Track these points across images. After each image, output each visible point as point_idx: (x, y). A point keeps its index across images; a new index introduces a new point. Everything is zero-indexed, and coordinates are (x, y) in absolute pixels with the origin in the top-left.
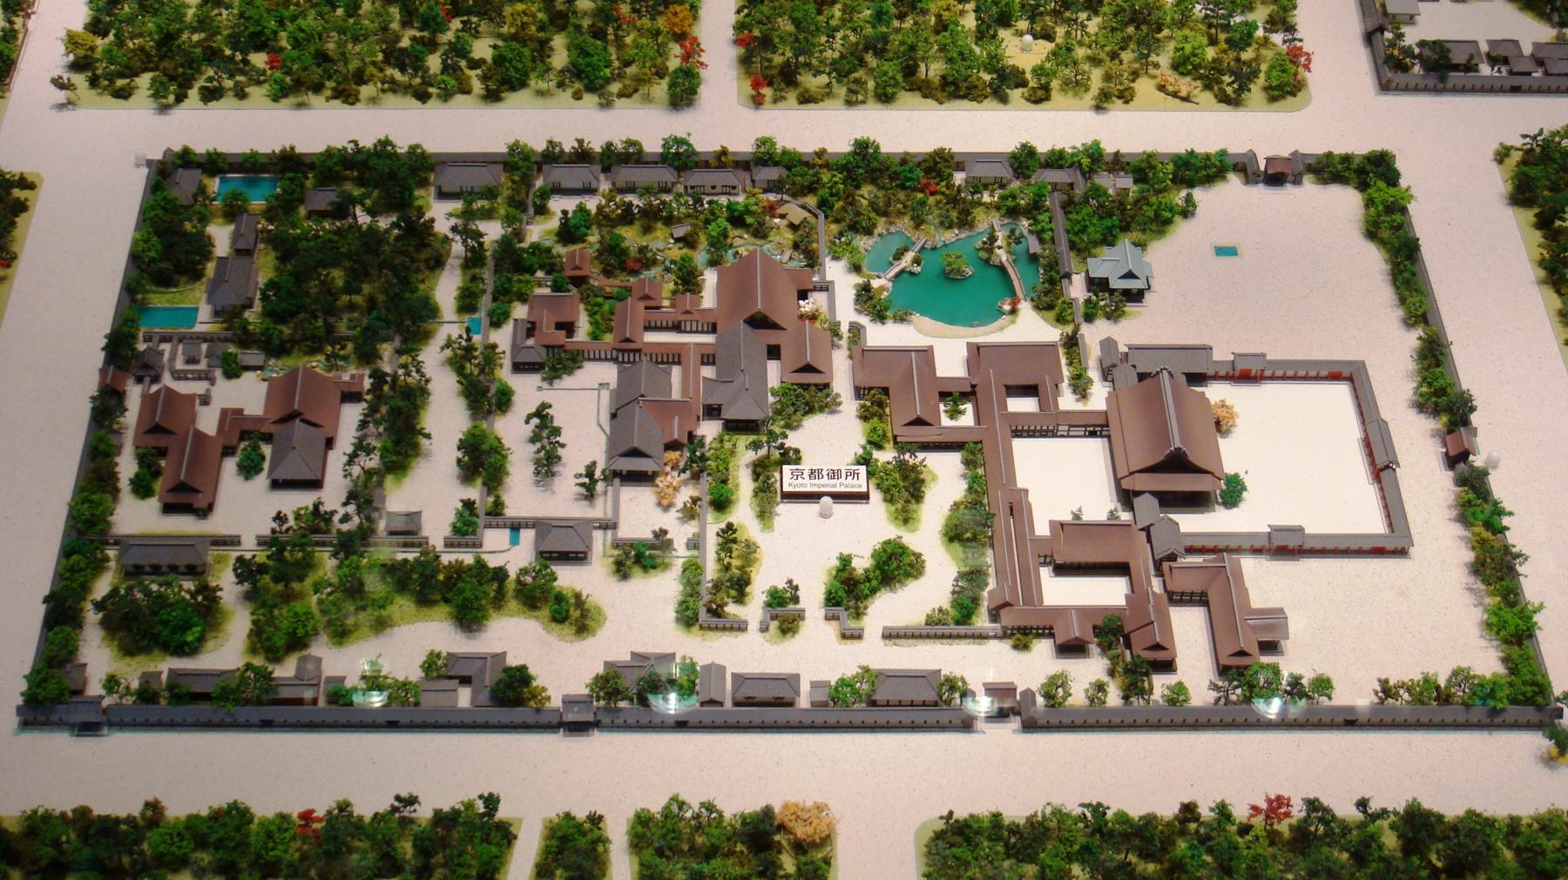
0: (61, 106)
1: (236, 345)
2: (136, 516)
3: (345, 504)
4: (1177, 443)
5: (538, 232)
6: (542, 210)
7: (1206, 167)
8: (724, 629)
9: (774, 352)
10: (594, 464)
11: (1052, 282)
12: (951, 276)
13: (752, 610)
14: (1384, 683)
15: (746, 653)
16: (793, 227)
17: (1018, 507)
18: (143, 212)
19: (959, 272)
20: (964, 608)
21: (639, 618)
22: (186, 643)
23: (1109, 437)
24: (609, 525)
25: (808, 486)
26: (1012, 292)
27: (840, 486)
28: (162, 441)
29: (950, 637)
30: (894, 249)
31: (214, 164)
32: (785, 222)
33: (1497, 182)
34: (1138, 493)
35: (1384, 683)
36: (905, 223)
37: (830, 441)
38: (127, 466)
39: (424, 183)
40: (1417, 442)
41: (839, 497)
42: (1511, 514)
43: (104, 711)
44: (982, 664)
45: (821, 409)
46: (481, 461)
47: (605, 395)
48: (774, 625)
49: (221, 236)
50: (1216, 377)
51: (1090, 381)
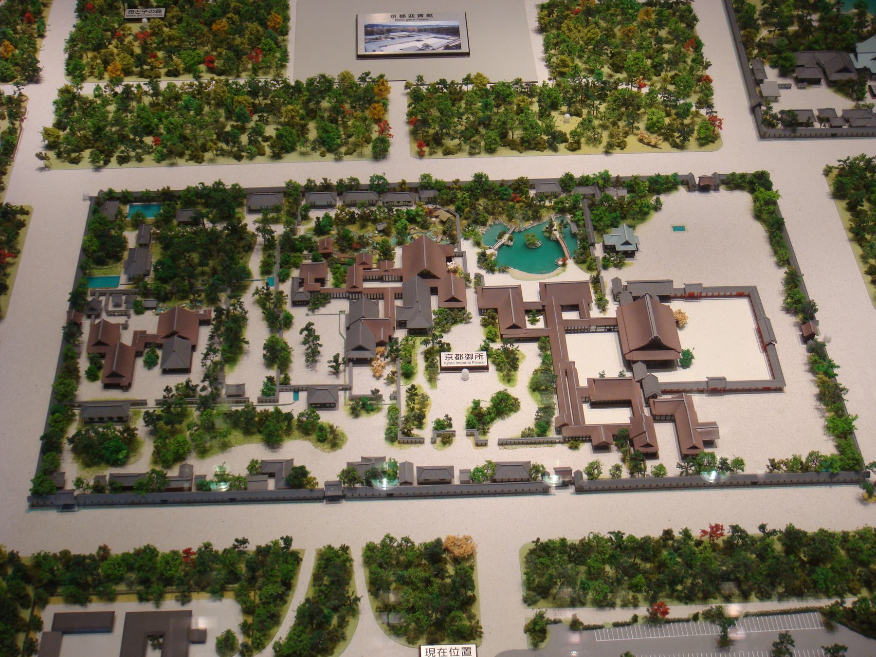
1: (141, 297)
2: (90, 391)
4: (656, 334)
5: (304, 229)
7: (666, 183)
8: (412, 443)
9: (434, 291)
10: (338, 355)
11: (584, 248)
12: (529, 247)
13: (427, 432)
14: (772, 461)
15: (424, 455)
17: (570, 371)
18: (88, 225)
19: (534, 244)
21: (365, 438)
23: (618, 332)
24: (347, 388)
25: (455, 363)
26: (563, 255)
27: (472, 363)
28: (103, 350)
29: (535, 443)
30: (498, 233)
31: (126, 198)
32: (438, 220)
33: (825, 187)
34: (635, 362)
35: (772, 461)
36: (503, 218)
37: (467, 339)
38: (84, 364)
39: (241, 205)
40: (785, 329)
41: (472, 369)
42: (838, 367)
44: (553, 457)
45: (461, 322)
46: (276, 355)
47: (343, 317)
48: (439, 440)
49: (131, 237)
51: (607, 302)
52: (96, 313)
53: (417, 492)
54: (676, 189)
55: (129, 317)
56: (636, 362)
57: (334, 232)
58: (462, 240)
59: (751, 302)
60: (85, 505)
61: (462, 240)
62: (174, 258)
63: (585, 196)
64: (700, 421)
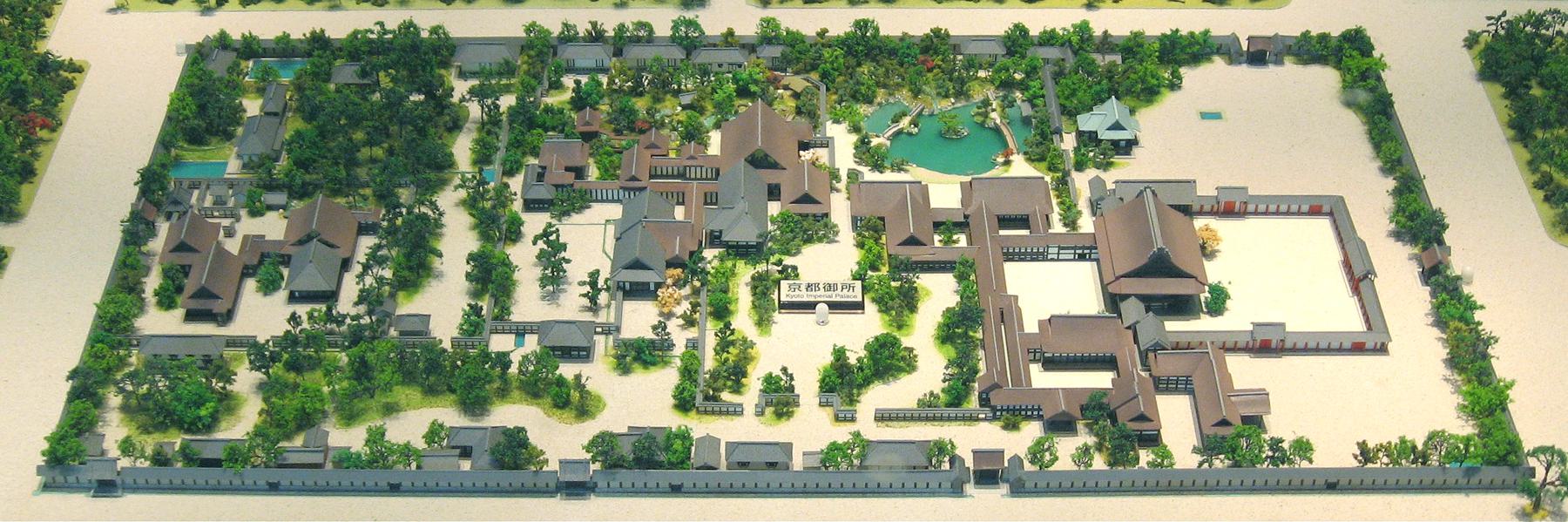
1: (261, 188)
2: (158, 322)
3: (356, 304)
4: (1159, 243)
5: (556, 99)
6: (556, 86)
7: (1191, 45)
8: (721, 413)
9: (774, 193)
10: (598, 271)
11: (1043, 135)
12: (948, 135)
13: (751, 396)
14: (1362, 446)
15: (745, 426)
16: (796, 96)
17: (1008, 313)
18: (182, 78)
19: (956, 132)
20: (956, 397)
21: (638, 402)
22: (200, 418)
23: (1097, 260)
25: (805, 297)
28: (185, 258)
29: (941, 419)
30: (894, 111)
31: (250, 48)
32: (789, 93)
33: (1467, 64)
34: (1125, 297)
35: (1362, 446)
36: (904, 96)
37: (830, 262)
38: (152, 282)
39: (445, 64)
40: (1397, 269)
41: (835, 306)
42: (1482, 307)
44: (971, 438)
45: (820, 240)
46: (490, 276)
47: (611, 229)
48: (769, 410)
49: (252, 106)
50: (1201, 213)
51: (1080, 213)
52: (181, 208)
54: (1209, 60)
57: (604, 108)
58: (829, 123)
59: (1334, 222)
60: (136, 489)
61: (829, 123)
63: (1046, 61)
64: (1237, 386)
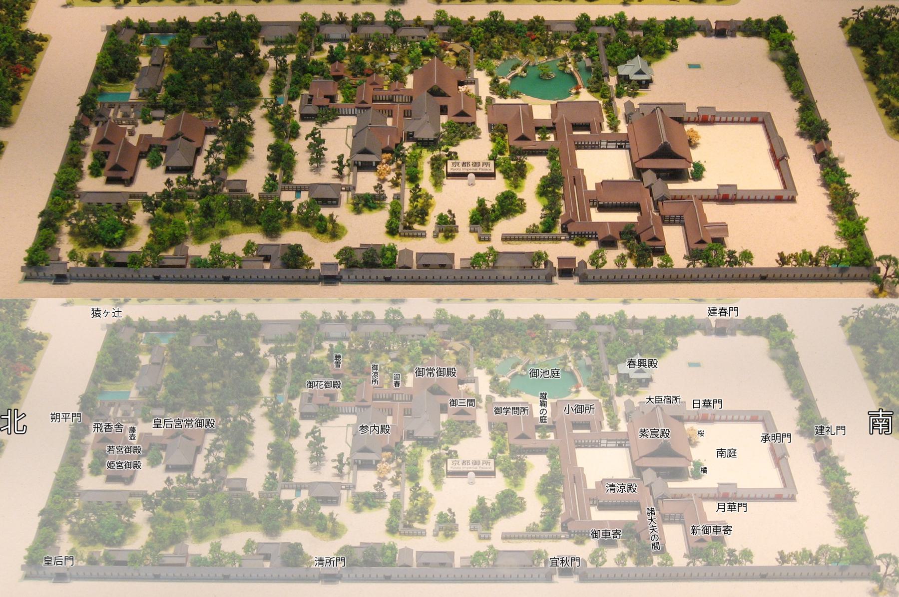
0: (65, 305)
1: (149, 108)
3: (204, 174)
4: (664, 139)
5: (319, 57)
6: (319, 49)
7: (683, 25)
9: (444, 110)
10: (343, 155)
11: (598, 376)
12: (544, 77)
13: (430, 226)
19: (548, 76)
23: (629, 149)
24: (349, 189)
26: (576, 83)
27: (479, 170)
28: (106, 148)
32: (452, 53)
37: (476, 449)
40: (801, 154)
43: (68, 271)
44: (557, 251)
48: (441, 235)
52: (104, 119)
53: (416, 277)
55: (137, 126)
56: (646, 170)
62: (185, 76)
